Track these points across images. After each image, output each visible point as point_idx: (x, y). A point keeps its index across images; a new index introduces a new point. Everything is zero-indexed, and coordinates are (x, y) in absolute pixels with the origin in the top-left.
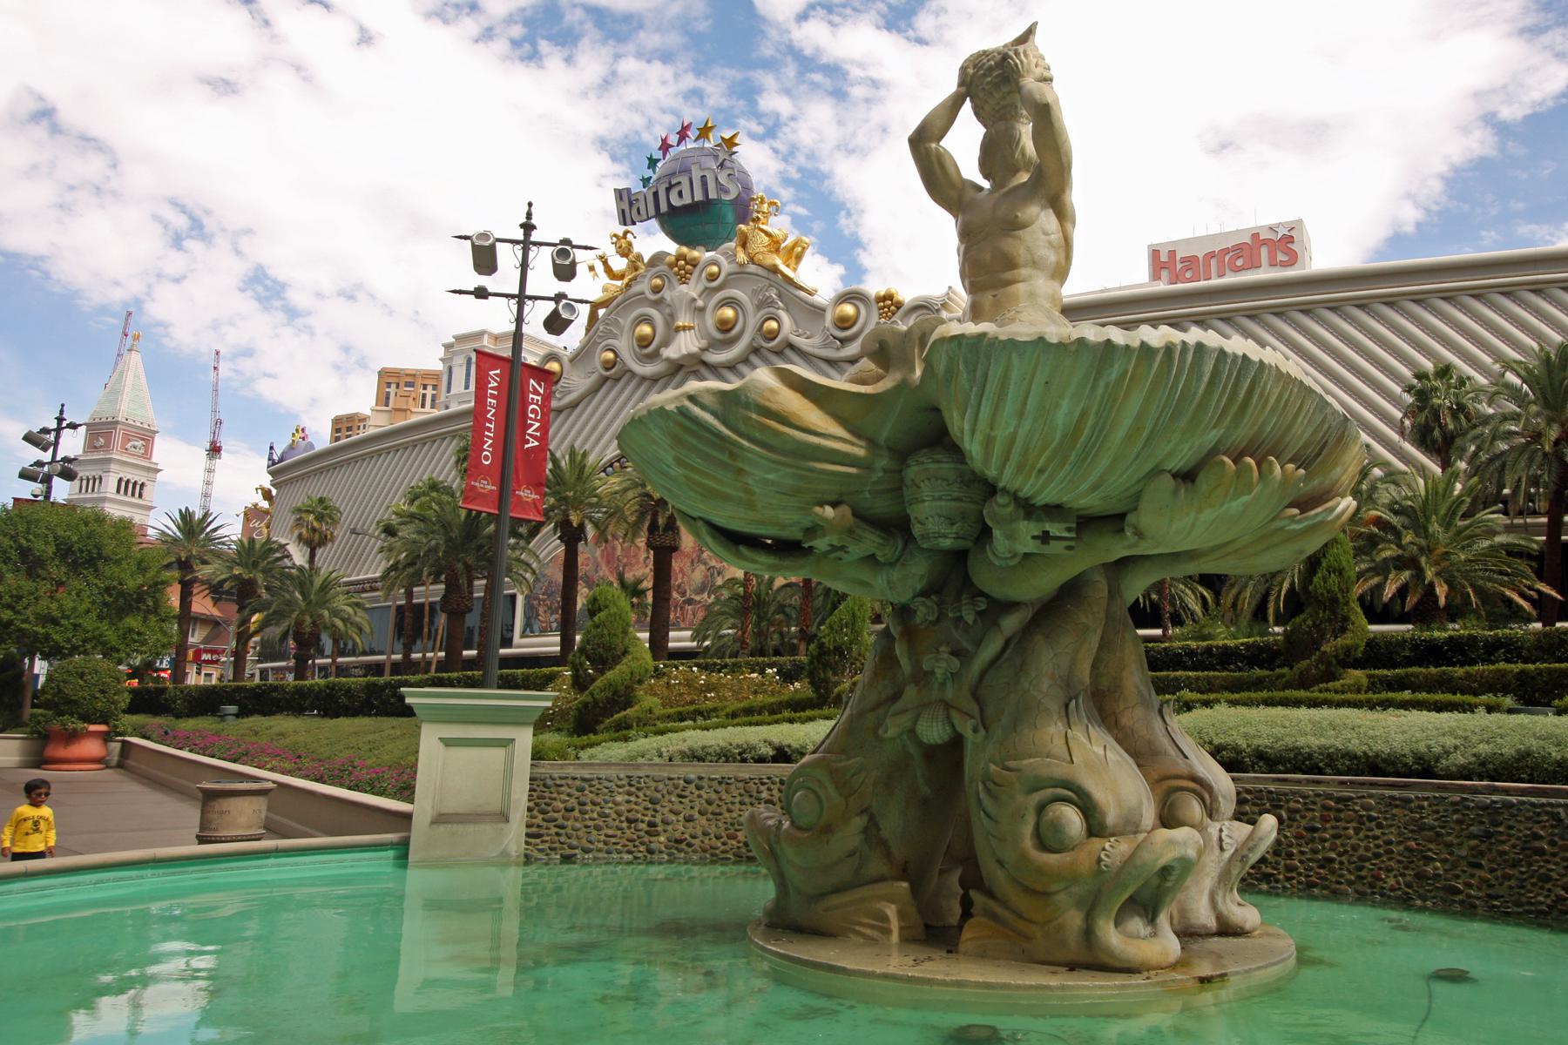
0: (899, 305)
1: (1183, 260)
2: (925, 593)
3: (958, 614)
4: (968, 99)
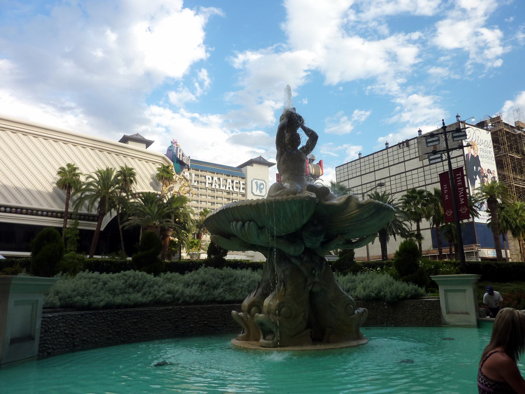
2: (303, 253)
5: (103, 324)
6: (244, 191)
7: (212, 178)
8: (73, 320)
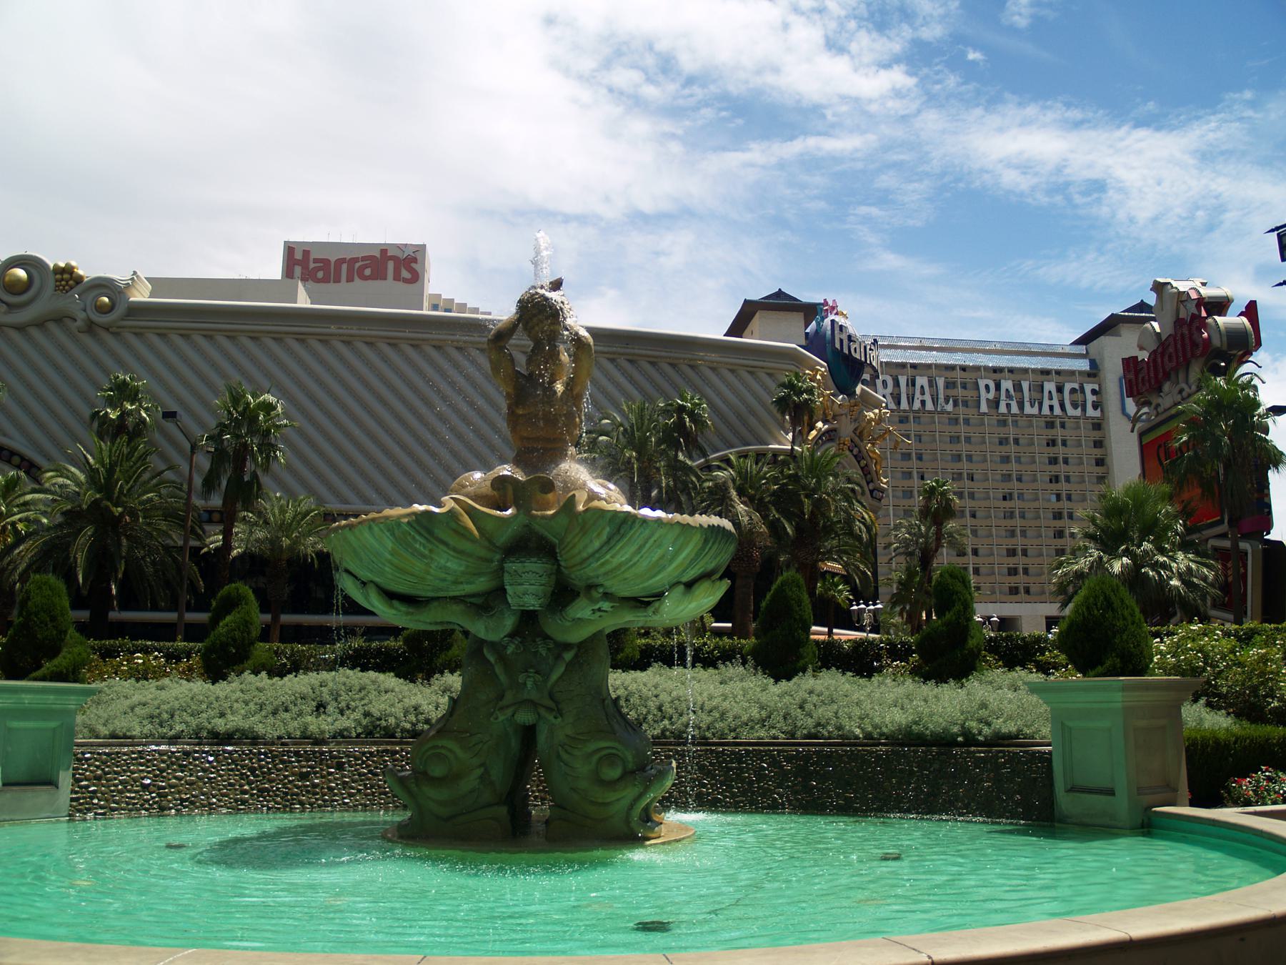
0: (79, 280)
1: (316, 261)
2: (512, 635)
6: (1097, 414)
7: (998, 387)
8: (163, 762)
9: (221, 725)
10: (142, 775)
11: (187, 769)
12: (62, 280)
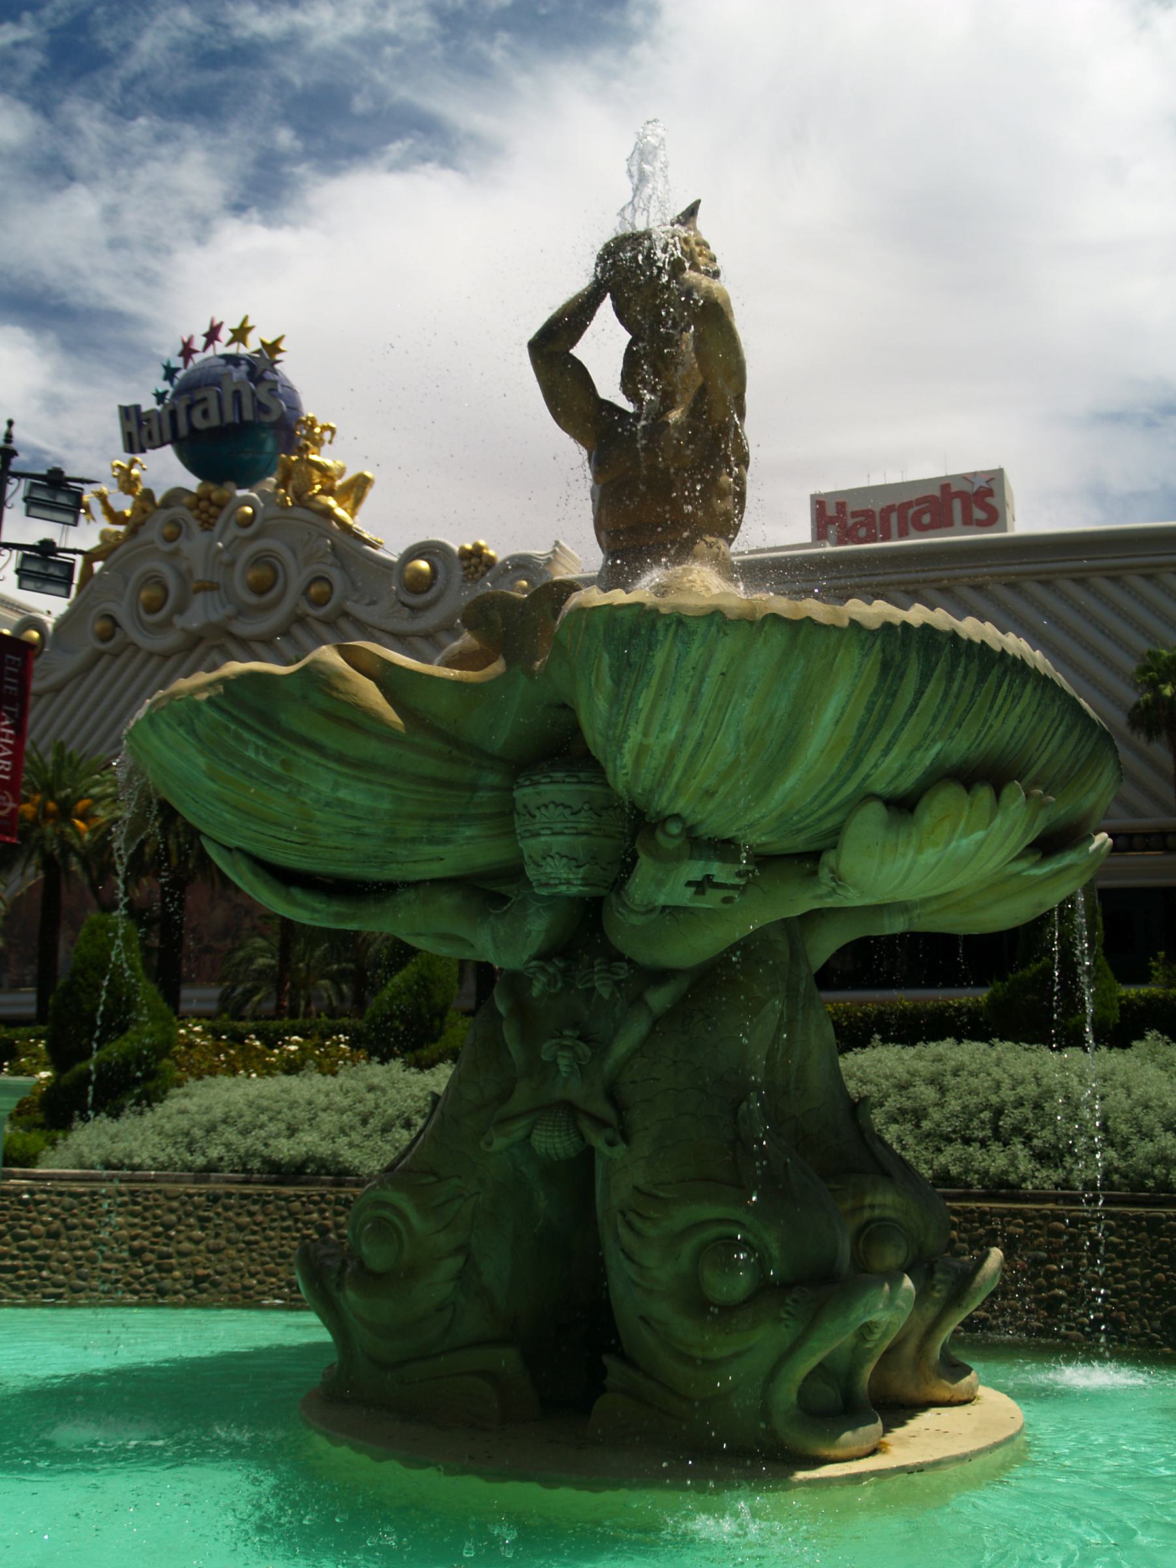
0: (490, 562)
1: (855, 514)
2: (544, 956)
3: (589, 985)
4: (609, 294)
5: (286, 1234)
8: (172, 1211)
9: (286, 1149)
10: (133, 1233)
11: (210, 1225)
12: (469, 567)
